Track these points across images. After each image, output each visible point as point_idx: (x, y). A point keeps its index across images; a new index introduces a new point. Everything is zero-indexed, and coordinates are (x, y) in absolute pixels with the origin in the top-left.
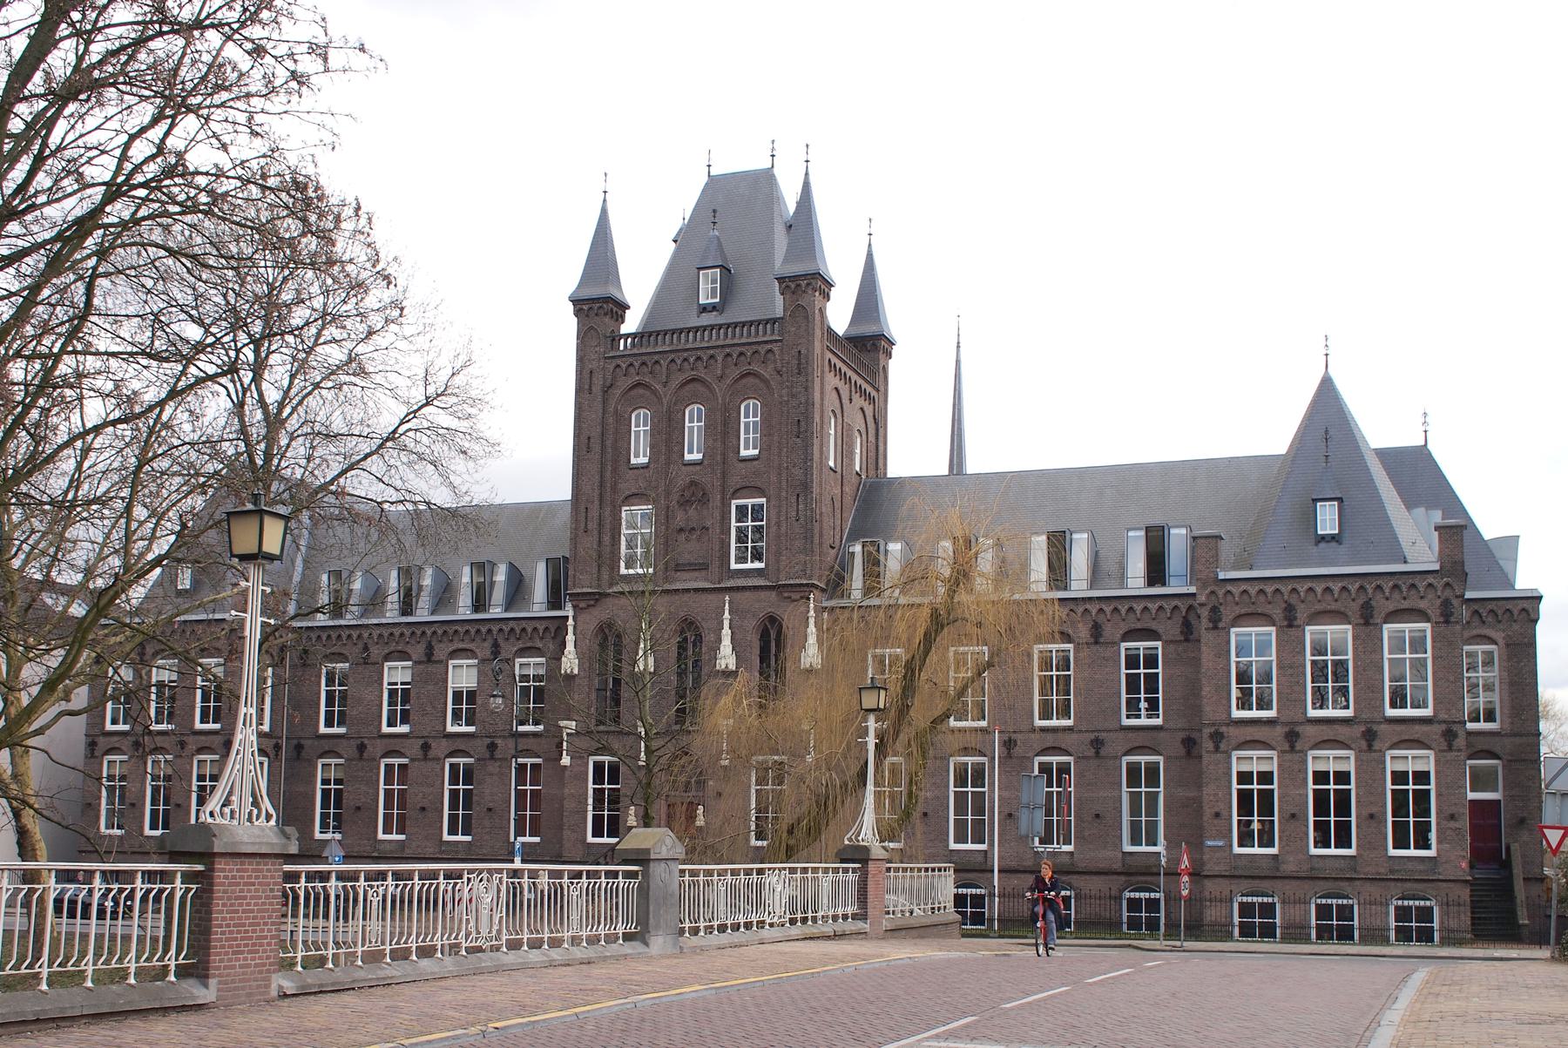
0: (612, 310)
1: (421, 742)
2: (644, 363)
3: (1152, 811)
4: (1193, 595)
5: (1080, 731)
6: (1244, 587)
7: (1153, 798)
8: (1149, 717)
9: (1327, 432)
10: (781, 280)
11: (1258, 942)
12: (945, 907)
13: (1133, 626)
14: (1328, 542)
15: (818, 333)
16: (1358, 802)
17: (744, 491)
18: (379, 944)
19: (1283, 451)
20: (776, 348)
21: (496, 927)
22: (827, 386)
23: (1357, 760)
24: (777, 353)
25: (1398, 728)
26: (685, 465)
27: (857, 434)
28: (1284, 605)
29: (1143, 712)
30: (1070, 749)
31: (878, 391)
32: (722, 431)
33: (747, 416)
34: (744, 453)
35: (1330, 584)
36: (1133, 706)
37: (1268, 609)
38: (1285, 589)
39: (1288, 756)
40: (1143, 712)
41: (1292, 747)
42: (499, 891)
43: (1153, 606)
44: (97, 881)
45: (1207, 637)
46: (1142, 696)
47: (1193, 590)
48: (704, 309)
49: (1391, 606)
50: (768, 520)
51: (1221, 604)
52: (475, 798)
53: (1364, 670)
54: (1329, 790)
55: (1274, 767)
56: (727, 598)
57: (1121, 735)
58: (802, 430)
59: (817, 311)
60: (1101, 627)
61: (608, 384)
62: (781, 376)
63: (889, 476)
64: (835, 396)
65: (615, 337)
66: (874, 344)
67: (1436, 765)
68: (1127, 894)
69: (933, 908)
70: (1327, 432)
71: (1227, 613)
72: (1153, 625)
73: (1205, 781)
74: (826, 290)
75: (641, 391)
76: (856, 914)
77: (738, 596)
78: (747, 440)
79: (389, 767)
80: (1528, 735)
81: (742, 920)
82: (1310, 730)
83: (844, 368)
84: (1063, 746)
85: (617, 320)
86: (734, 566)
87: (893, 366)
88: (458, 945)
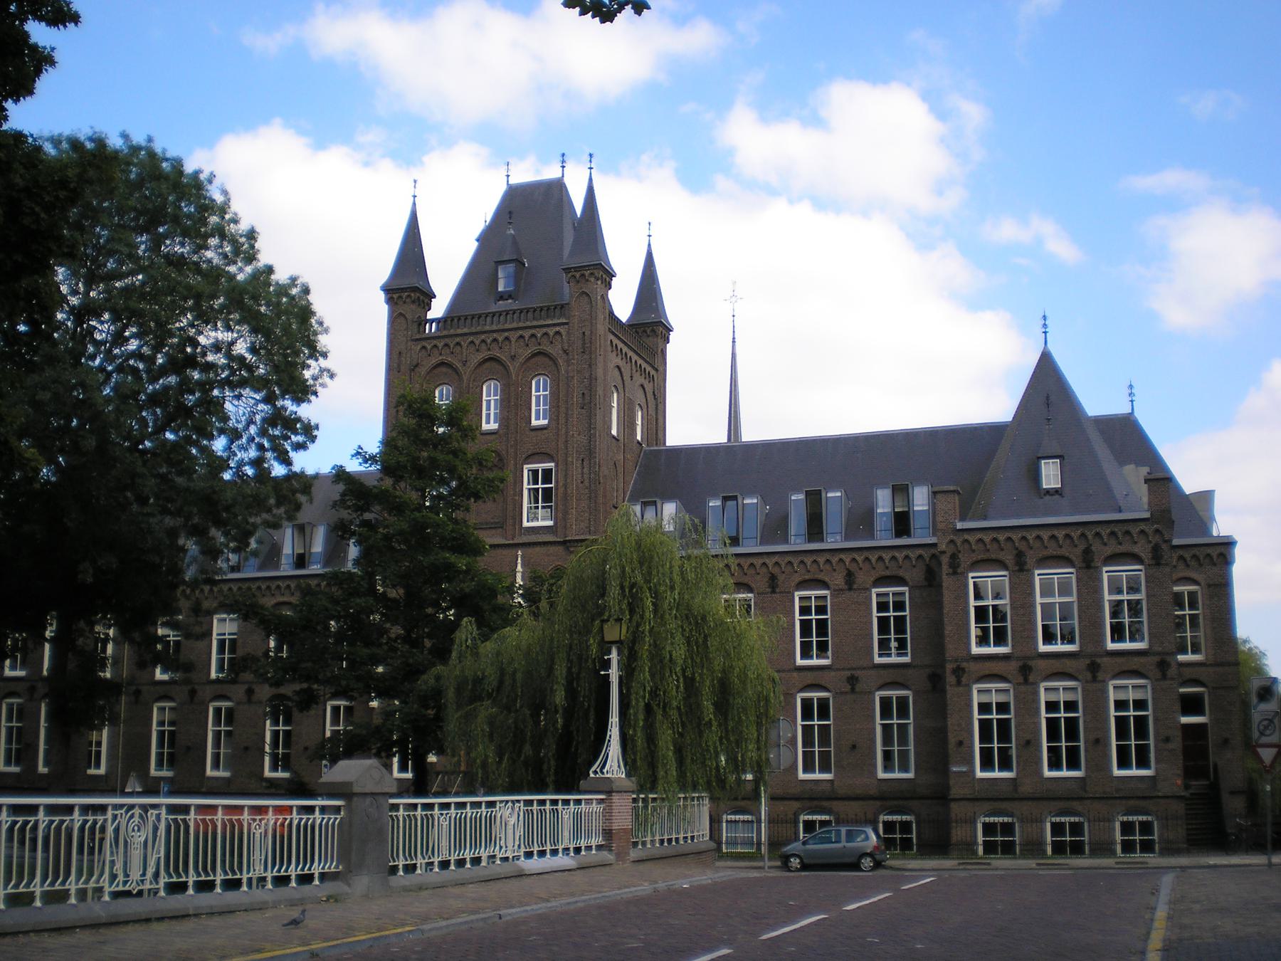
0: (419, 297)
1: (246, 687)
2: (458, 344)
3: (903, 740)
4: (934, 545)
5: (838, 670)
6: (979, 536)
7: (903, 728)
8: (899, 655)
9: (1048, 398)
10: (567, 270)
11: (1000, 858)
12: (693, 838)
13: (884, 573)
14: (1052, 495)
15: (601, 317)
16: (1085, 728)
17: (536, 457)
18: (262, 872)
19: (1090, 415)
20: (562, 330)
21: (517, 843)
22: (609, 362)
23: (1083, 691)
24: (564, 333)
25: (1120, 660)
26: (482, 434)
27: (637, 407)
28: (1015, 552)
29: (893, 650)
30: (828, 686)
31: (657, 370)
32: (514, 405)
33: (538, 390)
34: (534, 423)
35: (1056, 533)
36: (884, 645)
37: (1001, 556)
38: (1016, 536)
39: (1023, 688)
40: (893, 650)
41: (1026, 681)
42: (519, 815)
43: (900, 555)
44: (77, 812)
45: (947, 581)
46: (893, 636)
47: (933, 540)
48: (502, 297)
49: (1109, 550)
50: (557, 482)
51: (960, 552)
52: (294, 739)
53: (1088, 609)
54: (992, 719)
55: (1011, 698)
56: (520, 553)
57: (873, 672)
58: (586, 401)
59: (599, 298)
60: (853, 574)
61: (415, 363)
62: (567, 354)
63: (668, 444)
64: (618, 373)
65: (423, 322)
66: (653, 331)
67: (1153, 693)
68: (883, 818)
69: (686, 838)
70: (1048, 398)
71: (965, 559)
72: (901, 573)
73: (949, 712)
74: (608, 279)
75: (444, 369)
76: (602, 846)
77: (530, 550)
78: (538, 412)
79: (218, 711)
80: (1229, 664)
81: (468, 855)
82: (1042, 664)
83: (625, 349)
84: (823, 683)
85: (424, 308)
86: (526, 524)
87: (671, 349)
88: (99, 890)
